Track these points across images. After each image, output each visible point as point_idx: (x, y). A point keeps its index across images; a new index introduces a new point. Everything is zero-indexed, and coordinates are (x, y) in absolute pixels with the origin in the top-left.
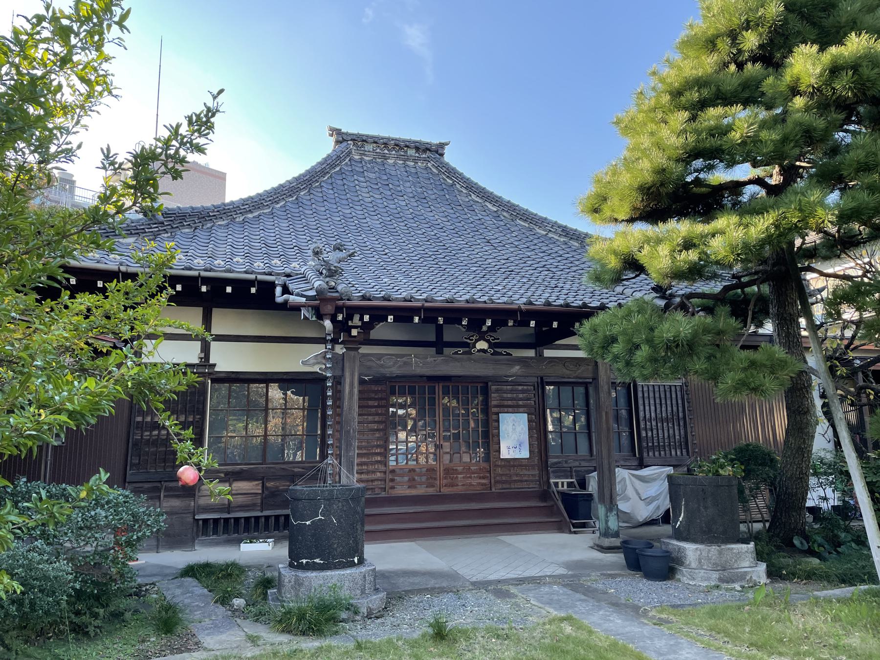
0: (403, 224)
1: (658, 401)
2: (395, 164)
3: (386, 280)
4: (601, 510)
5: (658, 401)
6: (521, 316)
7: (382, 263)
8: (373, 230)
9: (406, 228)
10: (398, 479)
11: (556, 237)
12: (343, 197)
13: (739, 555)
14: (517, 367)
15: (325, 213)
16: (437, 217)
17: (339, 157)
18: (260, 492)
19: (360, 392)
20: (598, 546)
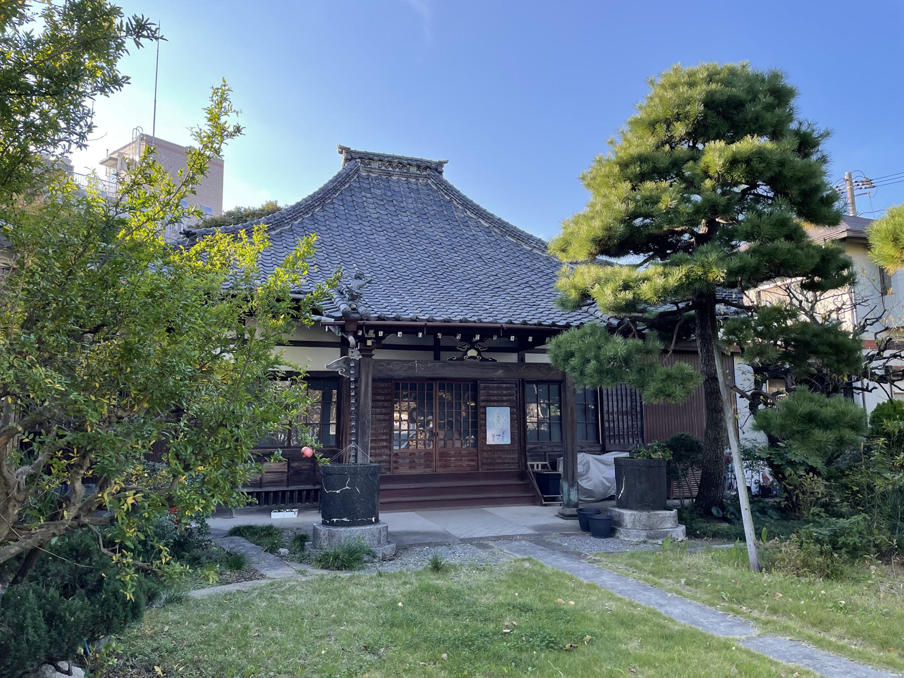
0: (406, 240)
1: (619, 398)
2: (398, 181)
3: (395, 300)
4: (565, 485)
5: (619, 398)
6: (505, 332)
7: (390, 281)
8: (381, 247)
9: (408, 244)
10: (400, 461)
11: (540, 253)
12: (352, 213)
13: (663, 520)
14: (501, 371)
15: (337, 230)
16: (436, 233)
17: (348, 175)
18: (286, 470)
19: (373, 388)
20: (561, 514)
